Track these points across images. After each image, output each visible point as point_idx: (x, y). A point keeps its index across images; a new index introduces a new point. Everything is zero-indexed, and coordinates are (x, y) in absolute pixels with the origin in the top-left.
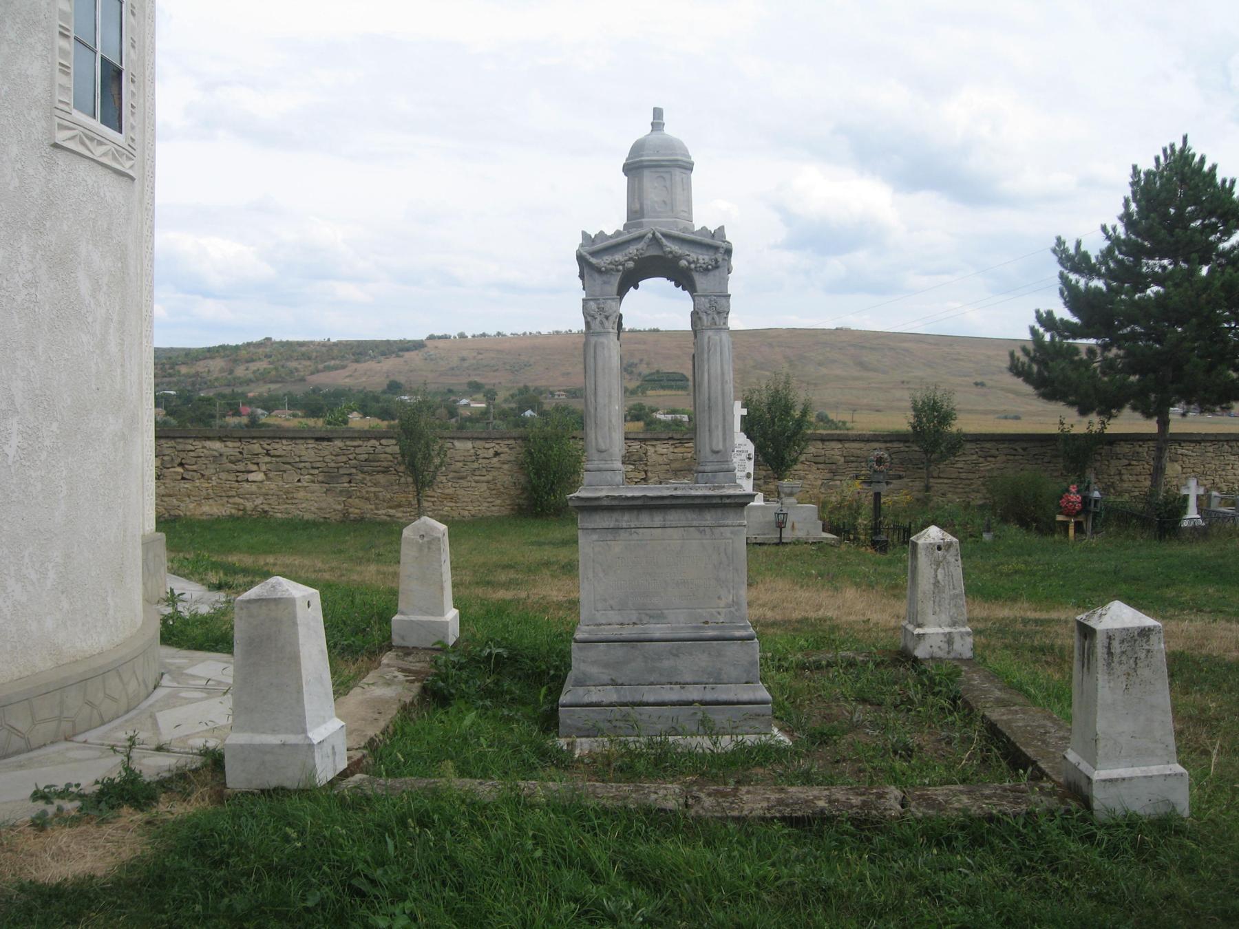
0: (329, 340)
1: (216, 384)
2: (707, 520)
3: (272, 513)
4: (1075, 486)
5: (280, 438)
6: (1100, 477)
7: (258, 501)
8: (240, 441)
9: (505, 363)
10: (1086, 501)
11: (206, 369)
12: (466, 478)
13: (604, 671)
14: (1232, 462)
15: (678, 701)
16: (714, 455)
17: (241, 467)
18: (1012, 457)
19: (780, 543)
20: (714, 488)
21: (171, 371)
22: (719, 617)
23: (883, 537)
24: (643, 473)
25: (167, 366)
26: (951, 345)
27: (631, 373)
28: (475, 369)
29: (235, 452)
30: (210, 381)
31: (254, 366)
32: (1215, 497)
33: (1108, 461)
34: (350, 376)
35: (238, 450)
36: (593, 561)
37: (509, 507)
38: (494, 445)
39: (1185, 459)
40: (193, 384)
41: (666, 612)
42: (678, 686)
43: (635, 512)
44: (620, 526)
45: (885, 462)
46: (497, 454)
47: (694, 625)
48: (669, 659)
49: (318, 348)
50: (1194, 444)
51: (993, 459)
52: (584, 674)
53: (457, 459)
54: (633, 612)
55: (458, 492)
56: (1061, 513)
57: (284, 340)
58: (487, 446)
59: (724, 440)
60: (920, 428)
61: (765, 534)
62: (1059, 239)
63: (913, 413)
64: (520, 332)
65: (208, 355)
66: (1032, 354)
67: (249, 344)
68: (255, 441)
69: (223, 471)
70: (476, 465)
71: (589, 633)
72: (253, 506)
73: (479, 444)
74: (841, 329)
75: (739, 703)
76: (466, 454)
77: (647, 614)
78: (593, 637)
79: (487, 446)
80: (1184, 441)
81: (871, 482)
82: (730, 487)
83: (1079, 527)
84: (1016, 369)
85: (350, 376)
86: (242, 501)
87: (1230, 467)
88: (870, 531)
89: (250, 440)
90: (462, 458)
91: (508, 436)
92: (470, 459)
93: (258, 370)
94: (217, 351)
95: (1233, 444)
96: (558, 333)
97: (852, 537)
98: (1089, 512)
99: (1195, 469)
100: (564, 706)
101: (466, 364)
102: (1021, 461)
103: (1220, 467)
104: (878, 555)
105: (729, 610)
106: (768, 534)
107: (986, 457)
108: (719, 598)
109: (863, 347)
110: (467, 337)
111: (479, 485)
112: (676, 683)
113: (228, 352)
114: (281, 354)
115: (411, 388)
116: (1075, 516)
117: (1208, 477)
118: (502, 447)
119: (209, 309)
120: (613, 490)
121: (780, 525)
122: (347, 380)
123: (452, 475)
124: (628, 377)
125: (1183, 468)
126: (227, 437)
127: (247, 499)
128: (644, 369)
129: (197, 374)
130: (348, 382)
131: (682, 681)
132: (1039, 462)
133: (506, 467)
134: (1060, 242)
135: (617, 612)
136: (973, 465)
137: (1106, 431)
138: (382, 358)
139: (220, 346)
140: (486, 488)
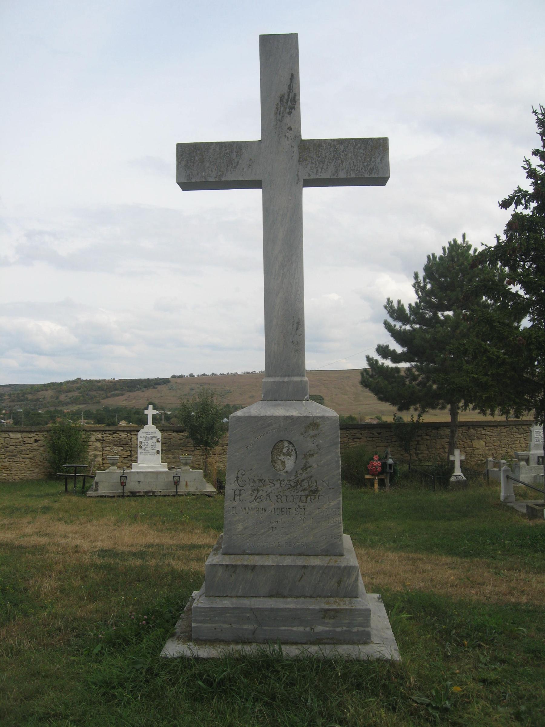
0: (114, 379)
1: (48, 405)
4: (377, 456)
6: (430, 450)
10: (384, 465)
11: (43, 397)
12: (17, 456)
14: (519, 439)
18: (371, 439)
19: (176, 495)
21: (22, 398)
24: (129, 452)
25: (20, 395)
31: (70, 395)
32: (491, 461)
33: (435, 440)
34: (126, 400)
37: (43, 474)
38: (34, 435)
39: (487, 437)
40: (35, 405)
46: (36, 441)
49: (108, 384)
50: (493, 428)
51: (358, 440)
53: (11, 444)
55: (11, 465)
56: (368, 474)
57: (88, 379)
58: (30, 436)
61: (167, 489)
62: (388, 299)
64: (225, 373)
65: (44, 388)
66: (370, 373)
67: (68, 382)
70: (23, 448)
73: (25, 435)
76: (17, 441)
79: (30, 436)
80: (486, 426)
83: (382, 483)
84: (365, 383)
85: (126, 400)
87: (518, 442)
90: (15, 444)
91: (43, 429)
92: (19, 444)
93: (73, 397)
94: (50, 386)
95: (520, 427)
96: (247, 373)
98: (387, 473)
99: (494, 444)
101: (193, 392)
102: (377, 441)
103: (511, 442)
106: (170, 489)
107: (354, 439)
110: (194, 376)
111: (24, 460)
113: (56, 387)
114: (86, 387)
115: (161, 406)
116: (378, 475)
117: (503, 449)
118: (39, 436)
119: (43, 362)
121: (177, 483)
122: (124, 402)
123: (8, 454)
125: (486, 443)
129: (38, 400)
130: (125, 403)
132: (389, 441)
133: (42, 449)
134: (389, 301)
136: (345, 444)
137: (421, 421)
138: (145, 389)
139: (51, 383)
140: (28, 462)
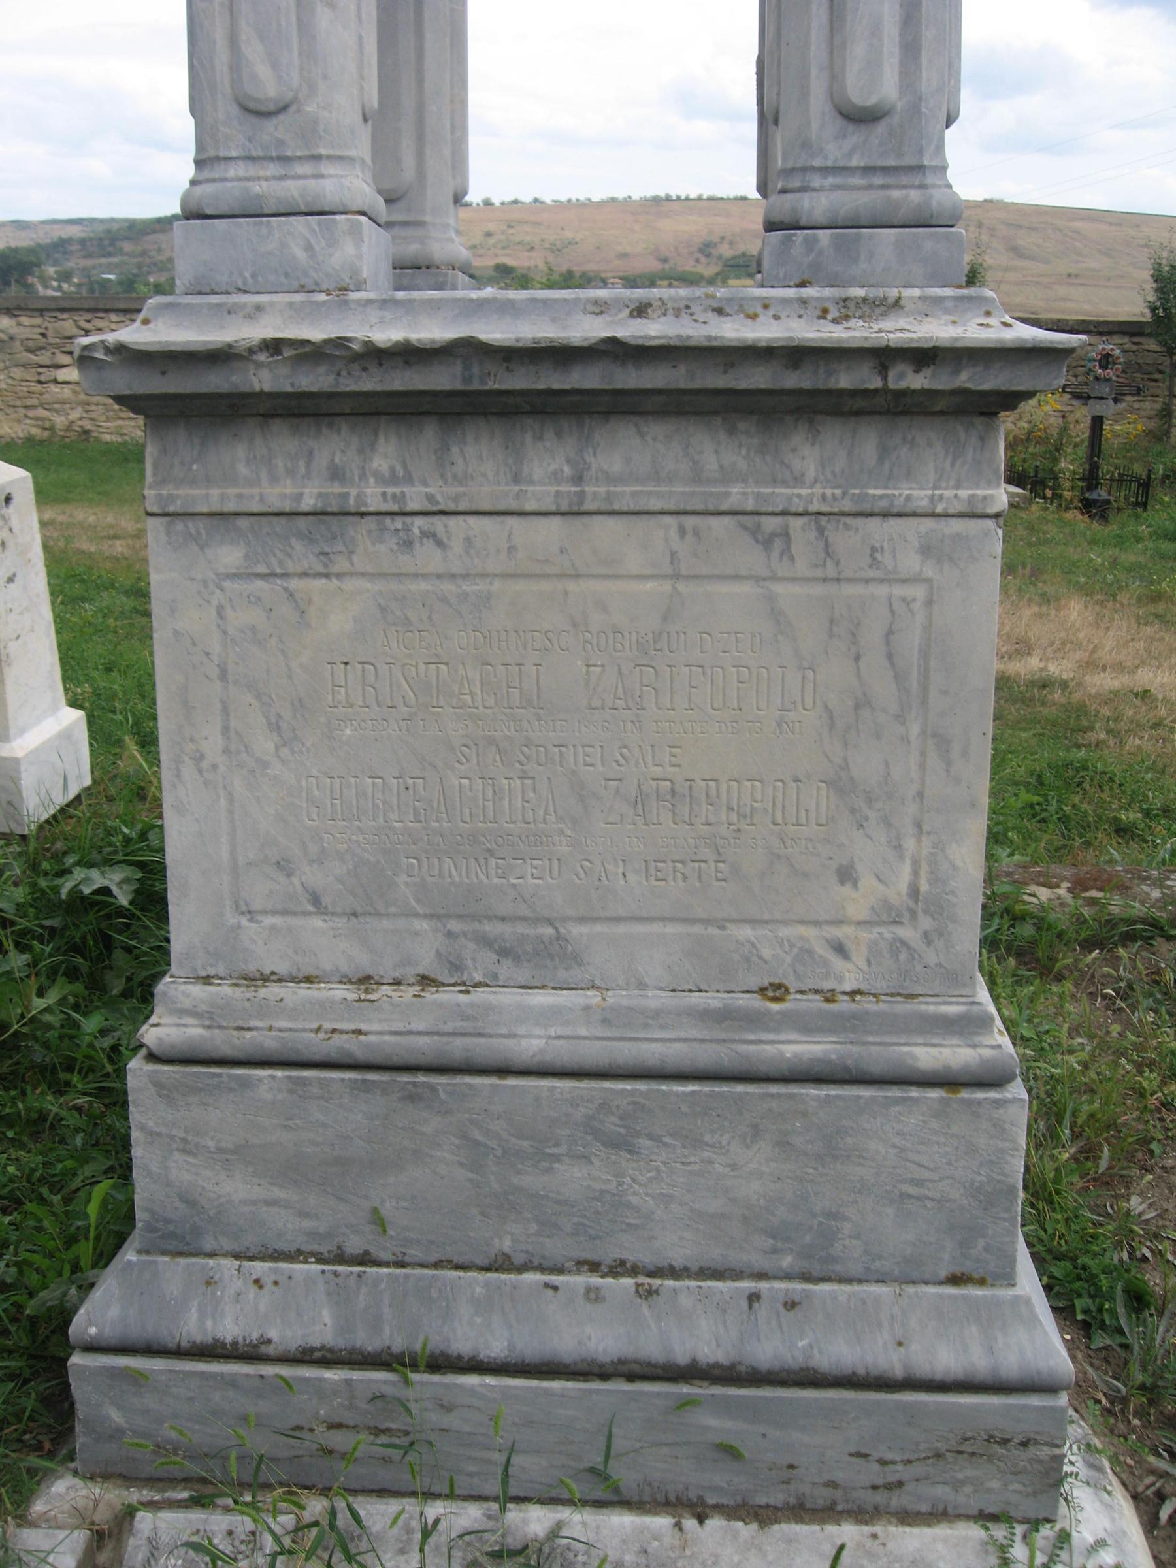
2: (798, 480)
3: (95, 434)
5: (106, 311)
7: (75, 415)
8: (42, 315)
9: (542, 240)
13: (278, 1193)
15: (621, 1362)
16: (855, 136)
17: (44, 358)
20: (847, 309)
22: (838, 963)
23: (1102, 494)
26: (1138, 226)
27: (708, 256)
28: (503, 248)
29: (34, 334)
30: (161, 262)
35: (40, 330)
36: (223, 675)
40: (139, 266)
41: (576, 931)
42: (628, 1282)
43: (430, 432)
44: (352, 505)
45: (1114, 363)
47: (713, 1000)
48: (586, 1158)
52: (191, 1203)
54: (422, 925)
59: (911, 49)
60: (1165, 310)
63: (1155, 285)
68: (65, 316)
69: (16, 366)
71: (209, 1017)
72: (66, 423)
74: (991, 201)
75: (911, 1384)
77: (485, 941)
78: (223, 1042)
81: (1089, 397)
82: (356, 1080)
86: (46, 414)
88: (1080, 483)
89: (58, 314)
97: (1049, 493)
100: (92, 1348)
104: (1095, 524)
105: (887, 932)
108: (846, 875)
109: (1020, 227)
112: (619, 1269)
120: (313, 312)
124: (703, 259)
126: (19, 308)
127: (57, 411)
128: (726, 251)
131: (646, 1258)
135: (340, 922)
